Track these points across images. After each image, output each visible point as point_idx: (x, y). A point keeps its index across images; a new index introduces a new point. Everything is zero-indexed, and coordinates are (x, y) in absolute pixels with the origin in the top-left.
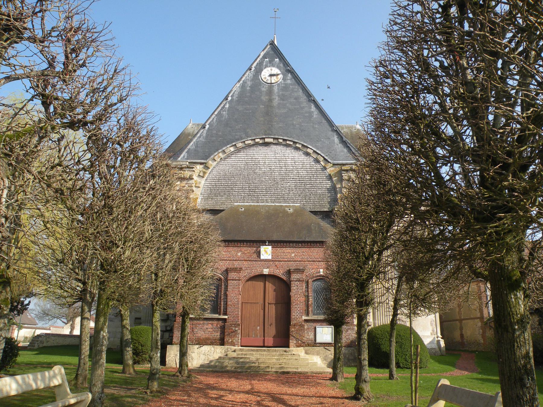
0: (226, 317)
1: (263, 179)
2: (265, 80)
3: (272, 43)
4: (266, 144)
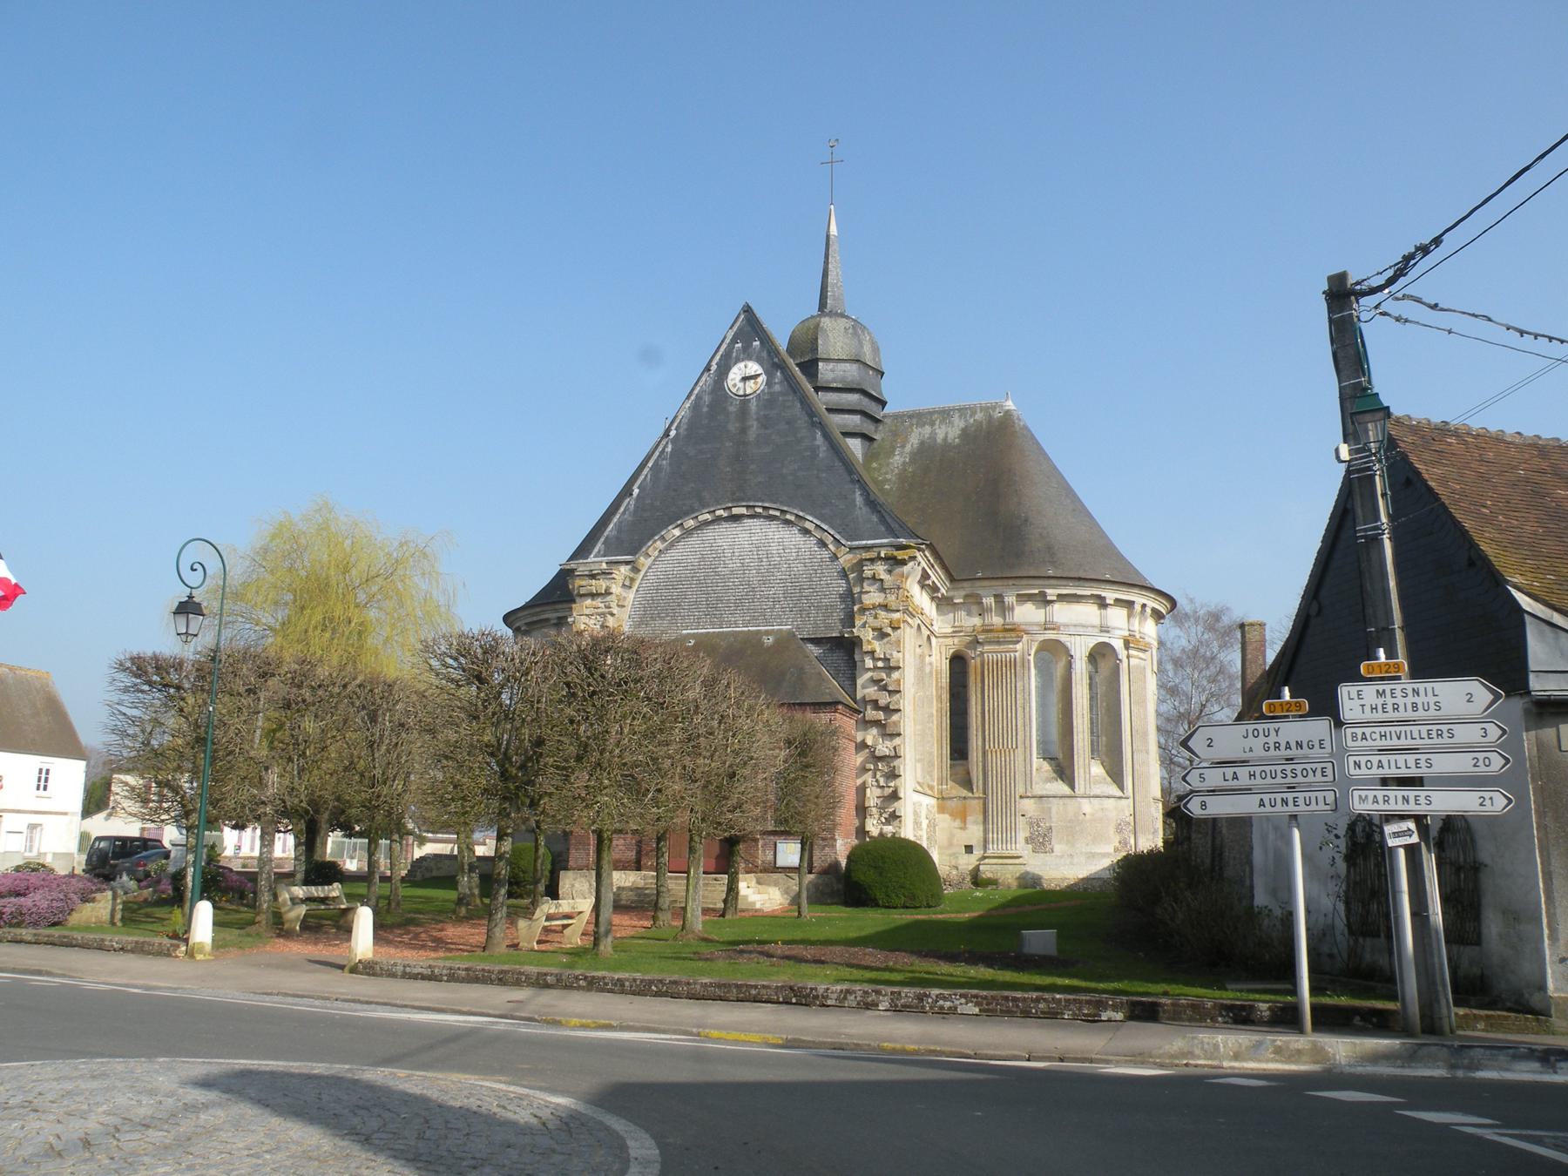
2: (734, 390)
3: (747, 310)
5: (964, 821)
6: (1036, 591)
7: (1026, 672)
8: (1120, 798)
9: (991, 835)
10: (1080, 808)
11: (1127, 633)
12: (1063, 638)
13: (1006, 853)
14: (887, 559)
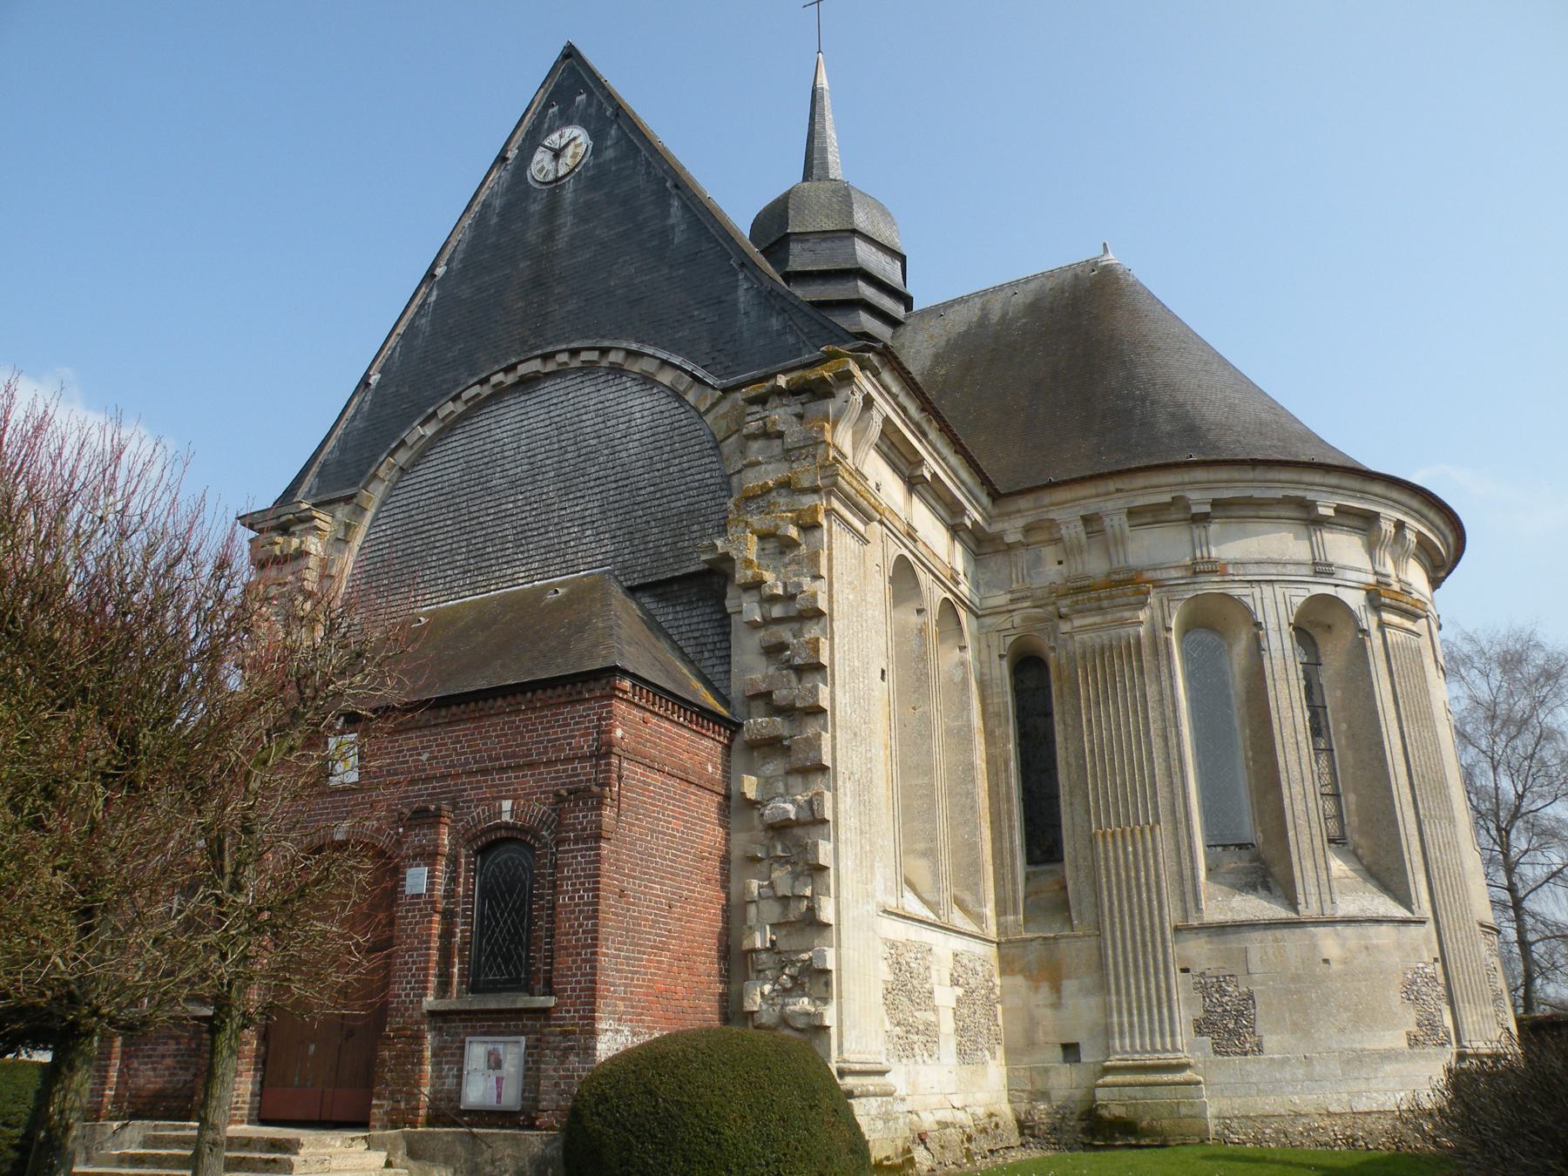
0: (551, 1001)
1: (511, 505)
3: (570, 53)
4: (528, 383)
5: (1057, 989)
6: (1167, 498)
7: (1164, 663)
8: (1405, 922)
9: (1115, 1019)
10: (1314, 947)
11: (1371, 579)
12: (1236, 591)
13: (1150, 1059)
14: (794, 391)
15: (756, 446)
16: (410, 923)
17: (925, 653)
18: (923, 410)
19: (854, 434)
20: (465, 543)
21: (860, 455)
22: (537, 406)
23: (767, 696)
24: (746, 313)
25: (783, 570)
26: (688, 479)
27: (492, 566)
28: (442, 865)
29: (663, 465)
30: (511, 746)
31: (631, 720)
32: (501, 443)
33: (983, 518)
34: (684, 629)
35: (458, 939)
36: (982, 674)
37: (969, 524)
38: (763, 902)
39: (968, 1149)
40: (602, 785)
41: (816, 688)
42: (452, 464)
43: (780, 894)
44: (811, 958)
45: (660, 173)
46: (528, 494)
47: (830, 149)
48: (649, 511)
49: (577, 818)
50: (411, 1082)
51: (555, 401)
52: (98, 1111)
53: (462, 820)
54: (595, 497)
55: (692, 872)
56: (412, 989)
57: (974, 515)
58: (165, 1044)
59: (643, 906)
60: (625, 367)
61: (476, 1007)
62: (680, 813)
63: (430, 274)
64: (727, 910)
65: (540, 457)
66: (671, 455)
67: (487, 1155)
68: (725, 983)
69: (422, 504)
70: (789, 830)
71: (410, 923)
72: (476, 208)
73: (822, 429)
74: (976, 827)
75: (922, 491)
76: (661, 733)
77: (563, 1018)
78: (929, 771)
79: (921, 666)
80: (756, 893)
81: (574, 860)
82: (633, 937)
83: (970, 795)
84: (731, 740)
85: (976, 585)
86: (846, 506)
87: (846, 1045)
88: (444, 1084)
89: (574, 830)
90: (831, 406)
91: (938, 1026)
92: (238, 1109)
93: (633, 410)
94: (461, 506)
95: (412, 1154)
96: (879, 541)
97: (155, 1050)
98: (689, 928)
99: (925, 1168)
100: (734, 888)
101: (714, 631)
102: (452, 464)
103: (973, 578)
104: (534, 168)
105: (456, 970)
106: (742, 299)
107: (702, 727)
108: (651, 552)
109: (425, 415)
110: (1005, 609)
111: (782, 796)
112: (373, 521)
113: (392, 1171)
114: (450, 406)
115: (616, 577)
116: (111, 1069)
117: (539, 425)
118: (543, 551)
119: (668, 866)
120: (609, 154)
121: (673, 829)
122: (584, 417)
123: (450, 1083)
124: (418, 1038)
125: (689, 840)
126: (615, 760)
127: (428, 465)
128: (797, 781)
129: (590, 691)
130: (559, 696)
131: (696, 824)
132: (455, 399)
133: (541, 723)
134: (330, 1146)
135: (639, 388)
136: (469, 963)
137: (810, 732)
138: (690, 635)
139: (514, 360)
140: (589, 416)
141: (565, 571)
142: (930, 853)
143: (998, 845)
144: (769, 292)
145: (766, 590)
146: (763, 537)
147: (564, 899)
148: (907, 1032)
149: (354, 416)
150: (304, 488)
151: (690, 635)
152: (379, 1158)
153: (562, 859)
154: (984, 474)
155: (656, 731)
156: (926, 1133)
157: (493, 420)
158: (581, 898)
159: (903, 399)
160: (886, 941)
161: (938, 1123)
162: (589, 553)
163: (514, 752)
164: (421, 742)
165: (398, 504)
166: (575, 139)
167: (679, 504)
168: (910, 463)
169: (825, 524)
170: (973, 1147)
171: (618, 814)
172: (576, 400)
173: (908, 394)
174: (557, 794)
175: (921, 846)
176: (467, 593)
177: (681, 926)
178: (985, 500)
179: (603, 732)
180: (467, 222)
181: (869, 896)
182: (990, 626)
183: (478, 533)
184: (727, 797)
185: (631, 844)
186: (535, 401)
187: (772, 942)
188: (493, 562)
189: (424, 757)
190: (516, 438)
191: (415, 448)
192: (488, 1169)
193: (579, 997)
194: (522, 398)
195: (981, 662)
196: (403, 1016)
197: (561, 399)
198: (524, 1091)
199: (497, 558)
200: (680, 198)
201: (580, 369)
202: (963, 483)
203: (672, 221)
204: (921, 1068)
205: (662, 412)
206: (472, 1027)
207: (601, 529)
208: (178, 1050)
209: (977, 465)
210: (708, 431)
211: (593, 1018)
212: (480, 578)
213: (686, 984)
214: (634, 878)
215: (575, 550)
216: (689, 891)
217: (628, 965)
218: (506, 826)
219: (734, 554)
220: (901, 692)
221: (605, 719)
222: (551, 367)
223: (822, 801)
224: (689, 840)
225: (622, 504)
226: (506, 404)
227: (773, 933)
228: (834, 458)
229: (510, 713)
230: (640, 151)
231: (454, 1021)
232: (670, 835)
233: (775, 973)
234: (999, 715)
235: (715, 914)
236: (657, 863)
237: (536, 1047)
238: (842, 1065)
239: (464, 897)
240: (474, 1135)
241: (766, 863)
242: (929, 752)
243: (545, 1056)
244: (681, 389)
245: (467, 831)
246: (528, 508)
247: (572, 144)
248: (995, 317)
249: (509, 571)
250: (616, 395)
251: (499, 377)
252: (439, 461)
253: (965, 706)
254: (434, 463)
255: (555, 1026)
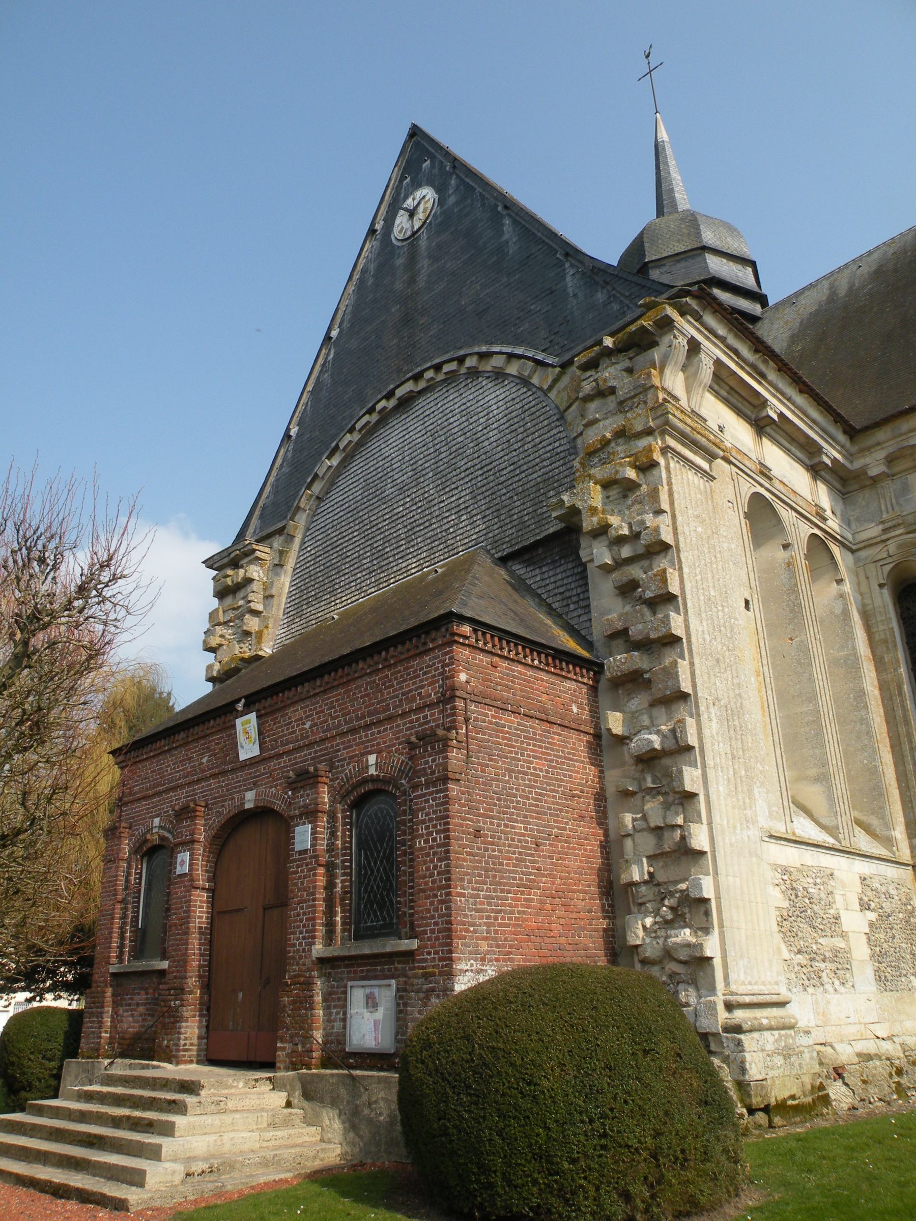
0: (414, 944)
1: (401, 508)
3: (415, 132)
4: (406, 403)
14: (619, 350)
15: (593, 406)
16: (300, 878)
17: (796, 585)
18: (756, 351)
19: (686, 379)
20: (368, 548)
21: (695, 399)
22: (415, 421)
23: (623, 633)
24: (575, 295)
25: (627, 512)
26: (541, 452)
27: (390, 563)
28: (323, 821)
29: (519, 444)
30: (373, 704)
31: (476, 665)
32: (390, 458)
33: (843, 456)
34: (551, 587)
35: (338, 889)
36: (864, 605)
37: (828, 462)
38: (637, 835)
39: (898, 1083)
40: (449, 729)
41: (667, 617)
42: (355, 485)
43: (652, 825)
44: (687, 889)
45: (492, 201)
46: (414, 496)
47: (676, 189)
48: (511, 488)
49: (427, 762)
50: (304, 1026)
51: (428, 413)
52: (98, 1050)
53: (338, 778)
54: (467, 486)
55: (561, 811)
56: (304, 938)
57: (832, 453)
58: (139, 994)
59: (504, 845)
60: (480, 369)
61: (353, 953)
62: (542, 753)
63: (327, 338)
64: (605, 847)
65: (420, 463)
66: (525, 434)
67: (365, 1097)
68: (609, 918)
69: (335, 523)
70: (657, 762)
71: (300, 878)
72: (356, 276)
73: (649, 375)
74: (874, 752)
75: (772, 433)
76: (514, 676)
77: (425, 960)
78: (812, 698)
79: (793, 598)
80: (630, 826)
81: (427, 806)
82: (495, 876)
83: (865, 721)
84: (597, 681)
85: (846, 522)
86: (683, 444)
87: (733, 977)
88: (333, 1027)
89: (425, 775)
90: (656, 354)
91: (849, 952)
92: (186, 1050)
93: (490, 404)
94: (363, 518)
95: (307, 1095)
96: (728, 480)
97: (132, 999)
98: (561, 865)
99: (845, 1106)
100: (612, 824)
101: (577, 584)
102: (355, 485)
103: (842, 515)
104: (396, 230)
105: (338, 919)
106: (570, 284)
107: (562, 669)
108: (515, 523)
109: (330, 449)
110: (879, 539)
111: (648, 728)
112: (301, 545)
113: (289, 1110)
114: (348, 437)
115: (488, 551)
116: (105, 1015)
117: (417, 436)
118: (429, 541)
119: (531, 805)
120: (452, 200)
121: (535, 769)
122: (452, 420)
123: (338, 1025)
124: (308, 985)
125: (557, 779)
126: (460, 704)
127: (337, 490)
128: (660, 713)
129: (433, 640)
130: (408, 650)
131: (563, 763)
132: (351, 430)
133: (396, 679)
134: (232, 1087)
135: (493, 383)
136: (350, 911)
137: (667, 662)
138: (556, 591)
139: (392, 386)
140: (455, 418)
141: (447, 555)
142: (823, 778)
143: (901, 768)
144: (592, 270)
145: (612, 533)
146: (606, 485)
147: (420, 842)
148: (811, 960)
149: (282, 466)
150: (251, 530)
151: (556, 591)
152: (280, 1098)
153: (417, 804)
154: (834, 410)
155: (507, 675)
156: (843, 1067)
157: (382, 441)
158: (434, 840)
159: (731, 340)
160: (775, 867)
161: (859, 1055)
162: (465, 535)
163: (375, 709)
164: (305, 712)
165: (318, 527)
166: (424, 197)
167: (535, 475)
168: (754, 407)
169: (662, 461)
170: (904, 1080)
171: (468, 756)
172: (444, 407)
173: (736, 336)
174: (409, 743)
175: (813, 772)
176: (373, 590)
177: (552, 864)
178: (842, 438)
179: (447, 678)
180: (351, 288)
181: (750, 821)
182: (866, 558)
183: (378, 538)
184: (597, 736)
185: (484, 784)
186: (413, 416)
187: (650, 873)
188: (391, 559)
189: (307, 726)
190: (400, 452)
191: (326, 478)
192: (366, 1111)
193: (437, 939)
194: (403, 417)
195: (861, 594)
196: (298, 964)
197: (432, 410)
198: (397, 1033)
199: (394, 555)
200: (509, 215)
201: (444, 380)
202: (814, 421)
203: (506, 237)
204: (833, 997)
205: (513, 399)
206: (355, 972)
207: (474, 512)
208: (147, 999)
209: (826, 402)
210: (553, 406)
211: (451, 959)
212: (382, 575)
213: (562, 921)
214: (491, 817)
215: (454, 535)
216: (559, 828)
217: (489, 904)
218: (372, 779)
219: (579, 505)
220: (772, 628)
221: (448, 665)
222: (422, 385)
223: (684, 727)
224: (557, 779)
225: (488, 487)
226: (391, 425)
227: (650, 865)
228: (664, 399)
229: (370, 673)
230: (474, 189)
231: (339, 967)
232: (532, 774)
233: (656, 905)
234: (885, 641)
235: (591, 851)
236: (518, 802)
237: (405, 990)
238: (729, 998)
239: (342, 849)
240: (351, 1076)
241: (639, 796)
242: (811, 679)
243: (410, 998)
244: (526, 374)
245: (342, 787)
246: (414, 507)
247: (423, 202)
248: (842, 291)
249: (404, 565)
250: (475, 394)
251: (383, 403)
252: (345, 485)
253: (849, 636)
254: (341, 488)
255: (419, 968)
